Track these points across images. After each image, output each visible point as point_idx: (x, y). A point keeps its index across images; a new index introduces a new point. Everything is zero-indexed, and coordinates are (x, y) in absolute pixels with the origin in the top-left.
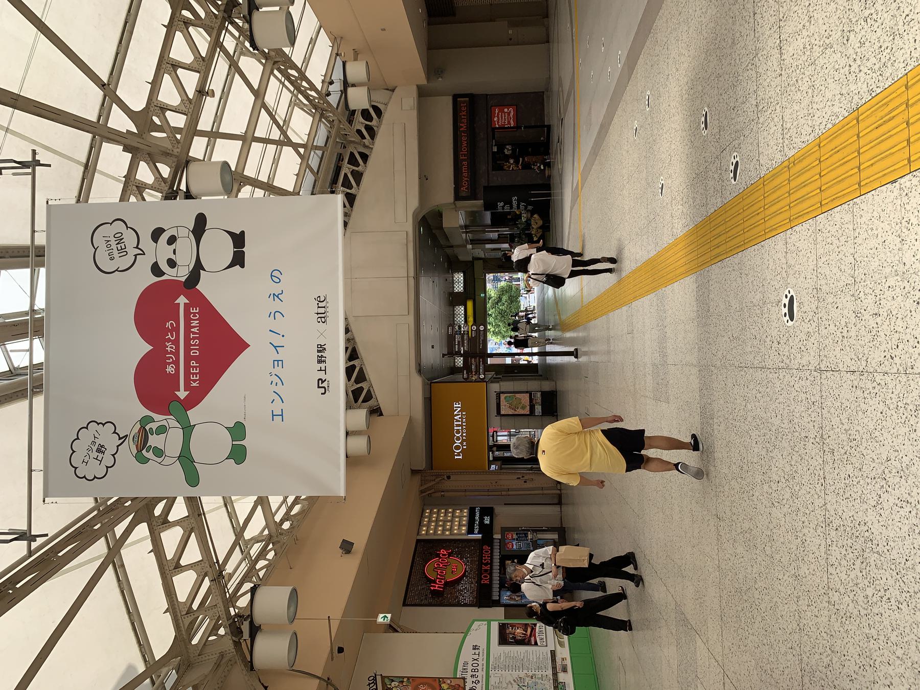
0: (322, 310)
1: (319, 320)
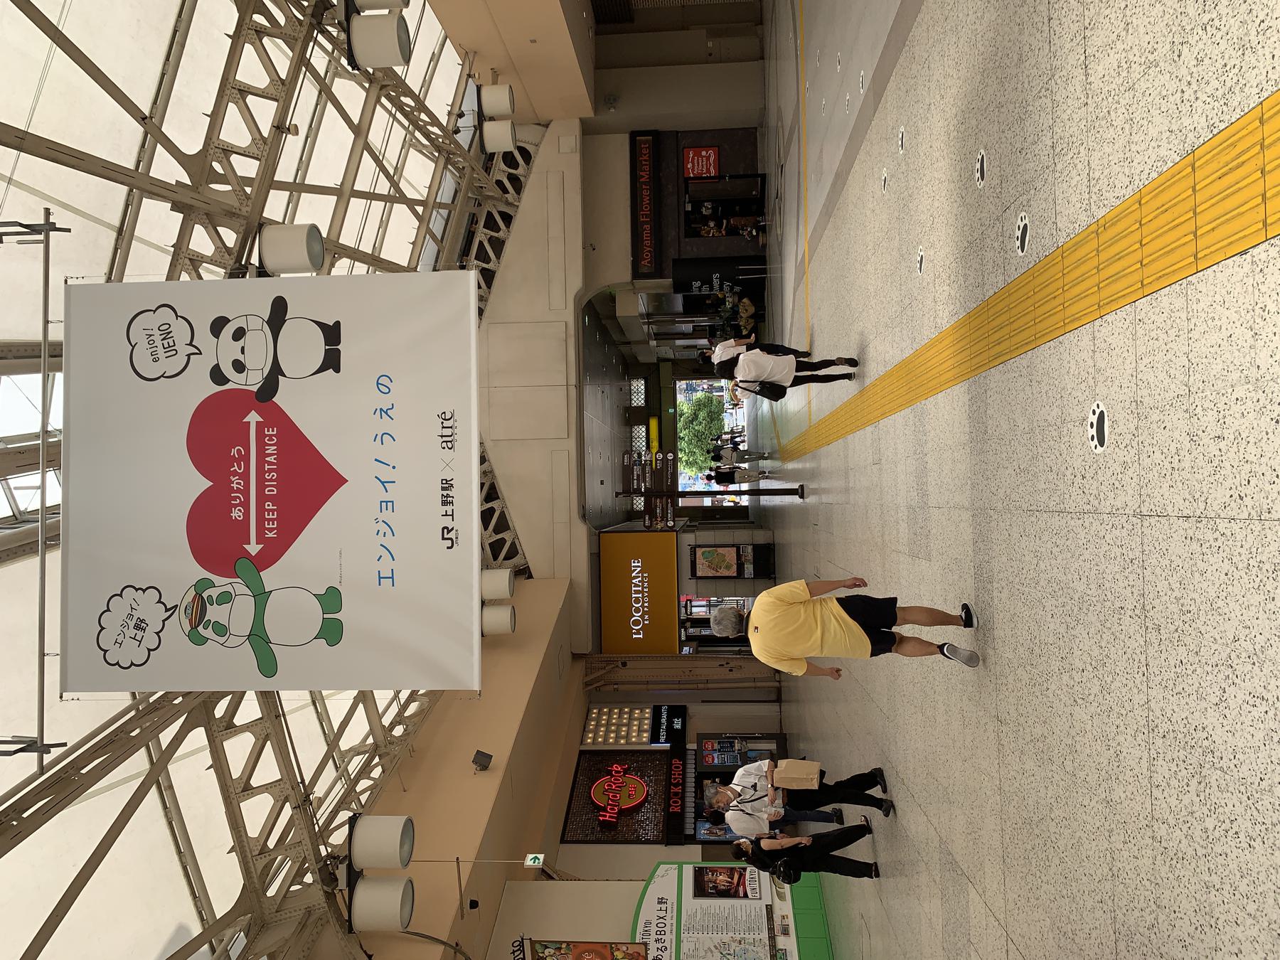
0: (448, 432)
1: (444, 445)
